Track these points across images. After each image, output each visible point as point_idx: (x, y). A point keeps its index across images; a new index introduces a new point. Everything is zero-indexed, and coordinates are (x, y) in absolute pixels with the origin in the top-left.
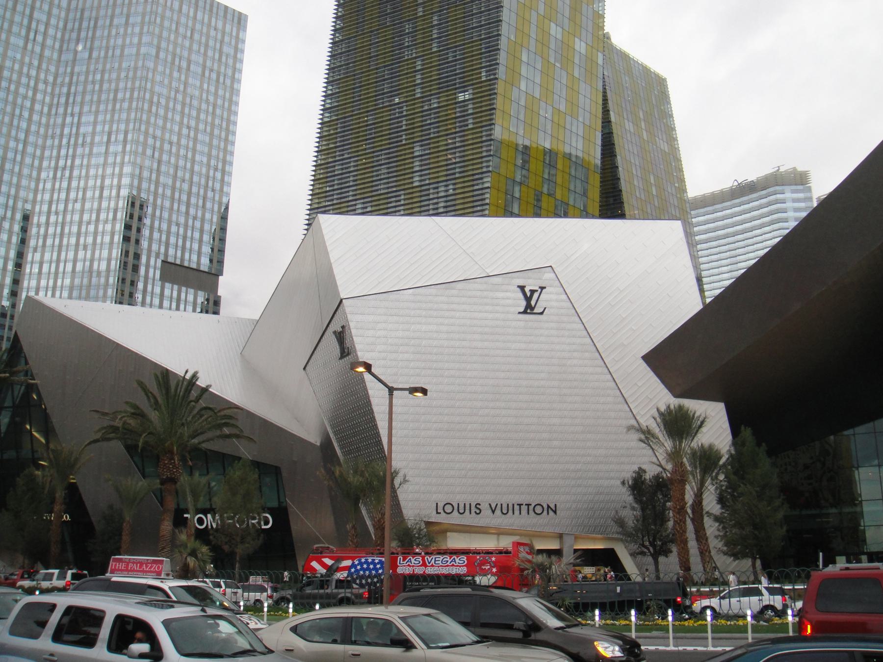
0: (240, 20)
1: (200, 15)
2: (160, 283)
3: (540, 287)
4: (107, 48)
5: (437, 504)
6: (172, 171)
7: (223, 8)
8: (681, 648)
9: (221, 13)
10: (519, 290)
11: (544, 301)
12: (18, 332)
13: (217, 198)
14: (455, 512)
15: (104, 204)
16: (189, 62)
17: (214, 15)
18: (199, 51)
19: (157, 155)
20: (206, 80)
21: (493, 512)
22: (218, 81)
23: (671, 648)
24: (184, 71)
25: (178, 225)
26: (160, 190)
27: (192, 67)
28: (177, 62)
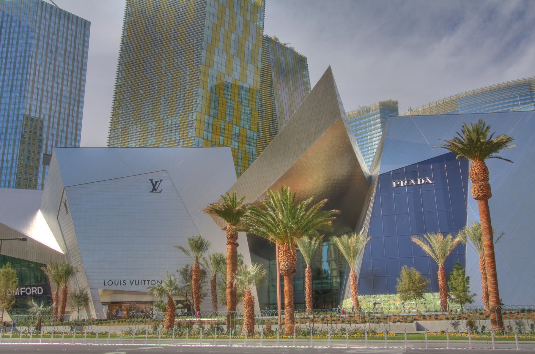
0: (86, 25)
1: (62, 22)
2: (42, 166)
3: (160, 180)
4: (9, 39)
5: (105, 281)
7: (75, 18)
8: (34, 344)
9: (75, 21)
10: (150, 181)
11: (161, 187)
13: (75, 121)
15: (10, 125)
16: (57, 47)
18: (62, 42)
21: (132, 284)
22: (74, 58)
23: (41, 344)
25: (53, 135)
27: (59, 51)
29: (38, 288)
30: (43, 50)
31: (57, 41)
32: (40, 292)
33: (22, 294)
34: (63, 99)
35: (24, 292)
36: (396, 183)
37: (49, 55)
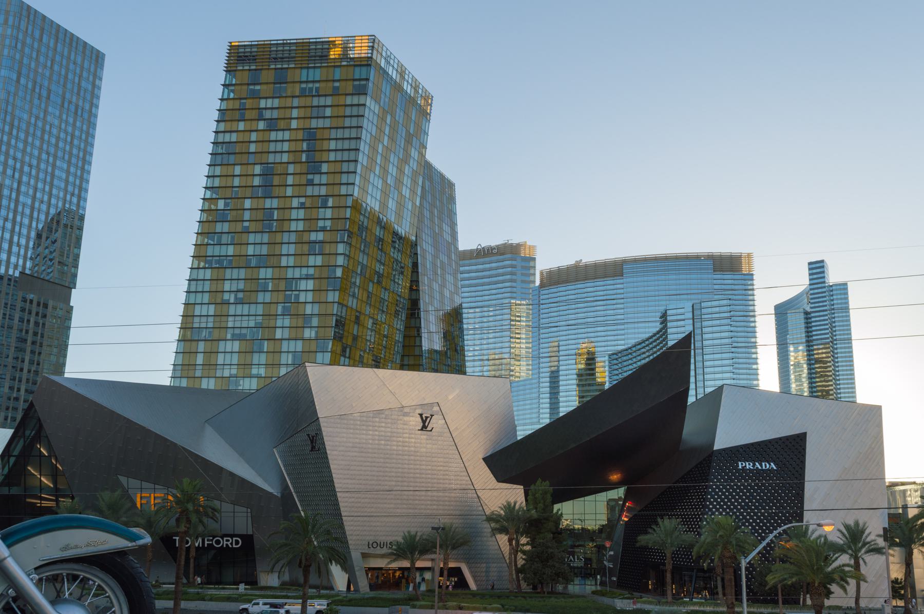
6: (31, 192)
9: (81, 48)
11: (436, 423)
12: (33, 401)
14: (379, 547)
16: (49, 91)
17: (74, 49)
19: (17, 175)
20: (65, 111)
24: (44, 100)
26: (20, 209)
28: (37, 90)
29: (234, 539)
30: (26, 92)
31: (50, 79)
32: (236, 545)
33: (206, 546)
34: (56, 182)
35: (211, 542)
36: (742, 464)
37: (36, 101)
